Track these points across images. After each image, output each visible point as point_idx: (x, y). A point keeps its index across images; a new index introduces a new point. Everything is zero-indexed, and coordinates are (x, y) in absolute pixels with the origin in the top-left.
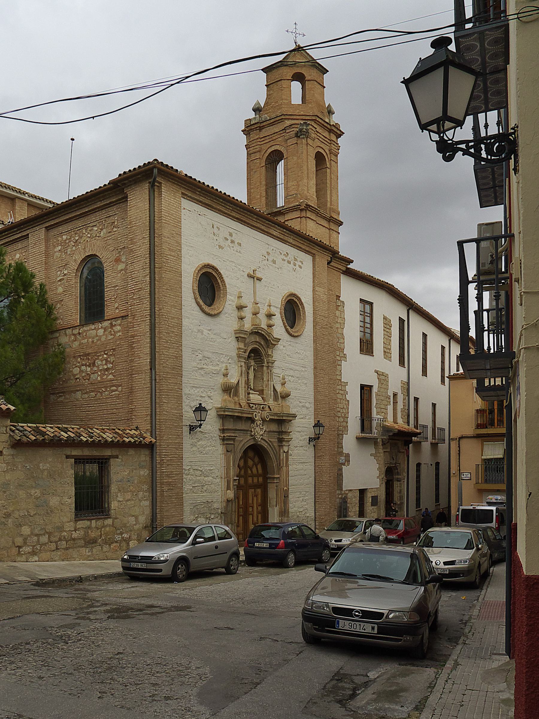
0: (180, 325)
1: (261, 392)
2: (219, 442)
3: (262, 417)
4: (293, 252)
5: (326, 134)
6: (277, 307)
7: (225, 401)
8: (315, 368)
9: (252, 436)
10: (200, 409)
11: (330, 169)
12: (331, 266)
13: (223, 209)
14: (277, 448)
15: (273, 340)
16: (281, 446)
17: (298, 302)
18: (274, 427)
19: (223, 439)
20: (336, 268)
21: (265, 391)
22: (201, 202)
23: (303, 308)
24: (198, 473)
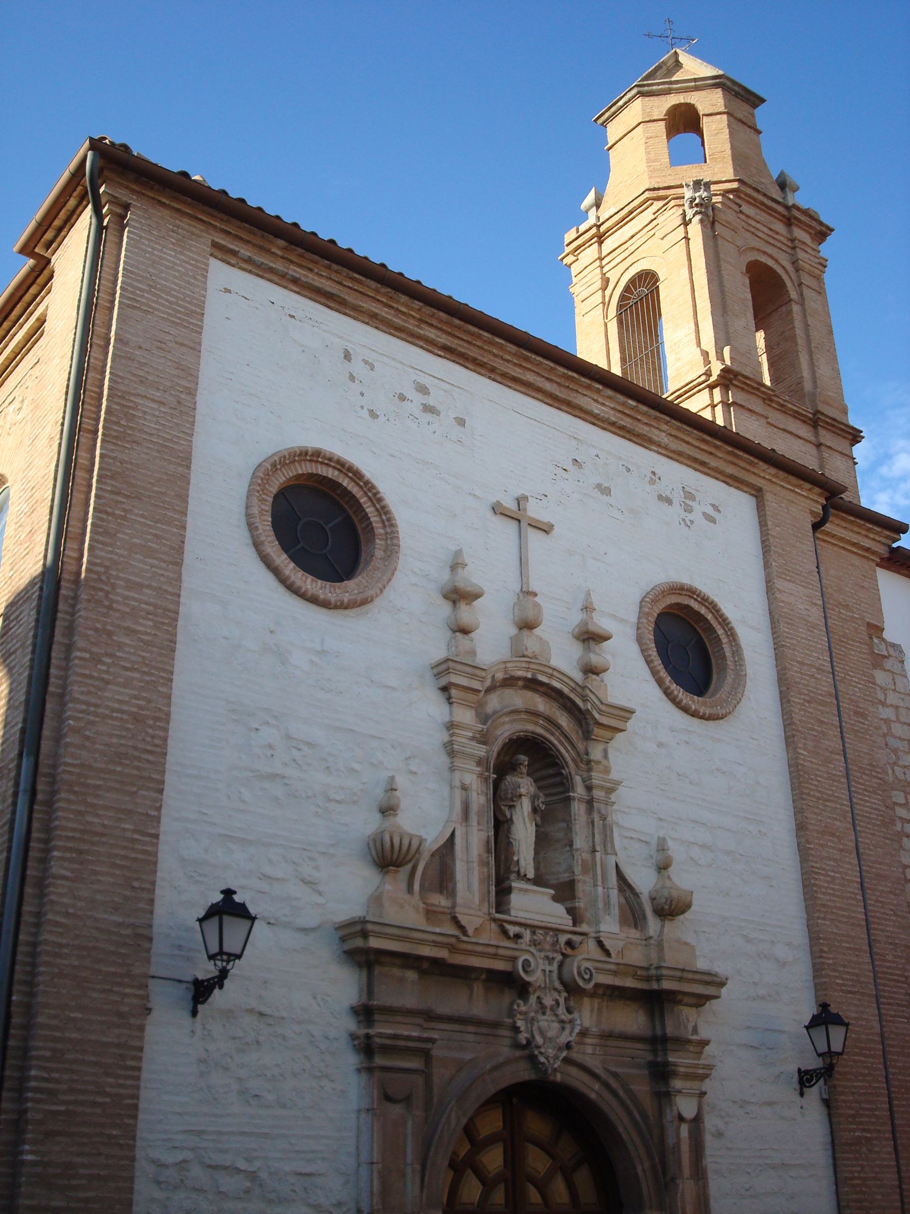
0: (167, 615)
1: (565, 892)
2: (351, 1060)
3: (566, 976)
4: (677, 475)
5: (780, 227)
6: (622, 620)
7: (377, 900)
8: (801, 827)
9: (517, 1046)
10: (228, 908)
11: (802, 304)
12: (828, 534)
13: (384, 312)
14: (648, 1103)
15: (600, 712)
16: (664, 1096)
17: (709, 617)
18: (631, 1020)
19: (366, 1048)
20: (854, 544)
21: (580, 888)
22: (295, 281)
23: (732, 634)
24: (230, 1183)
